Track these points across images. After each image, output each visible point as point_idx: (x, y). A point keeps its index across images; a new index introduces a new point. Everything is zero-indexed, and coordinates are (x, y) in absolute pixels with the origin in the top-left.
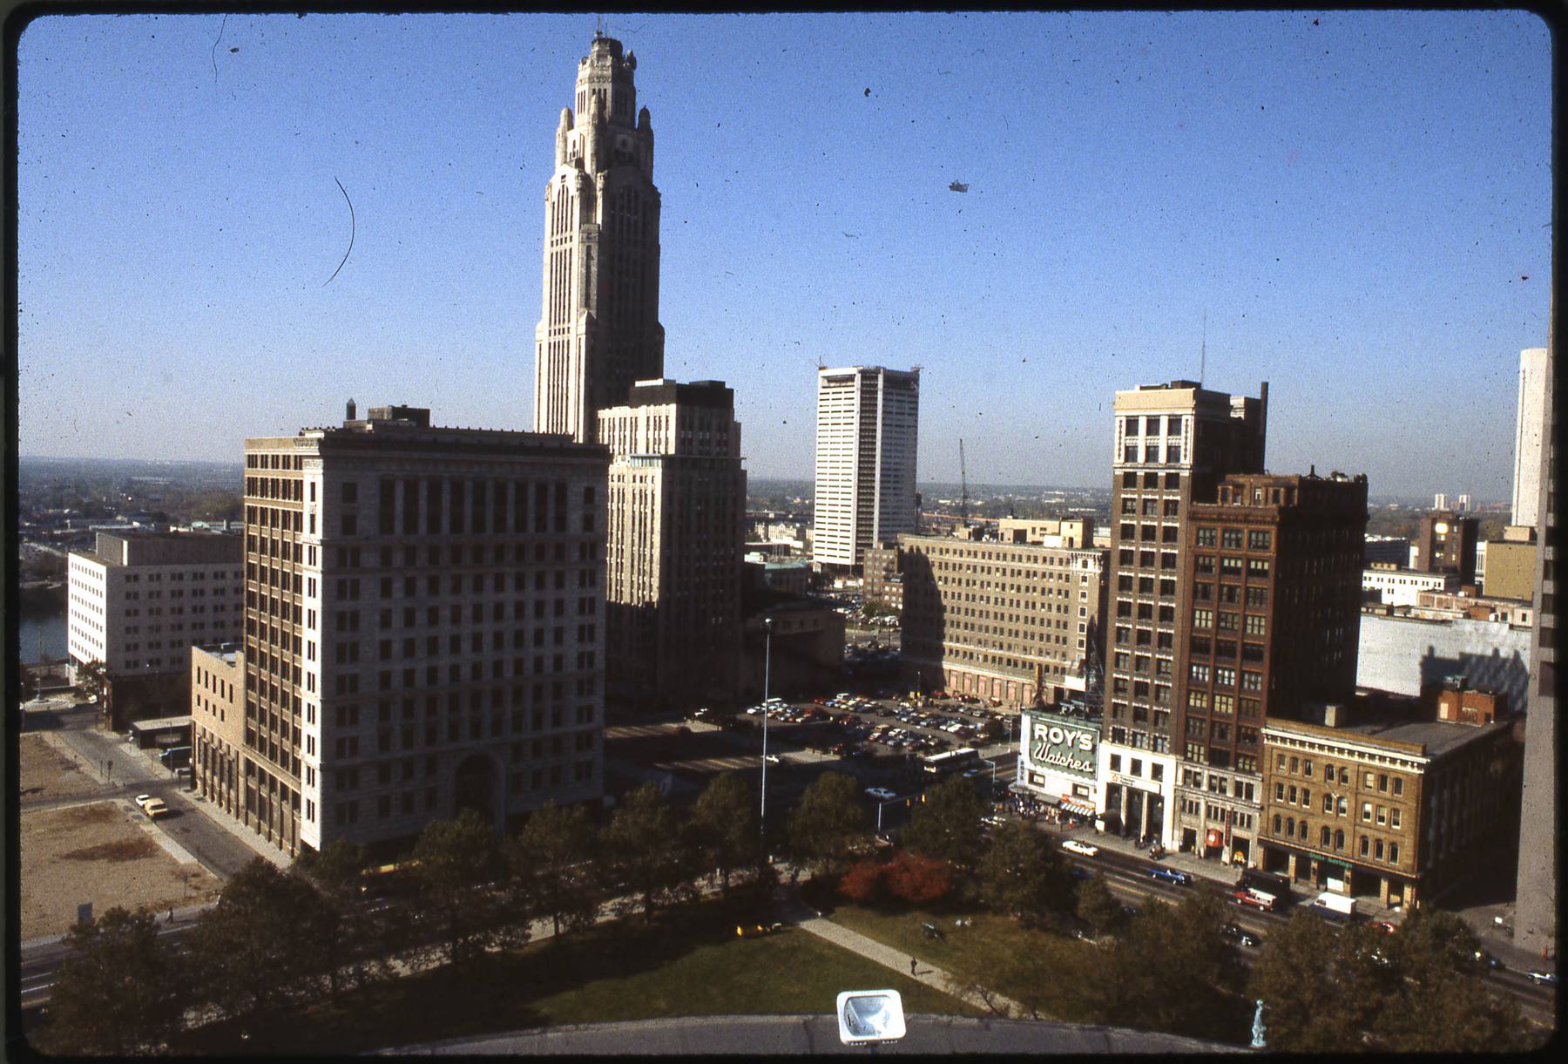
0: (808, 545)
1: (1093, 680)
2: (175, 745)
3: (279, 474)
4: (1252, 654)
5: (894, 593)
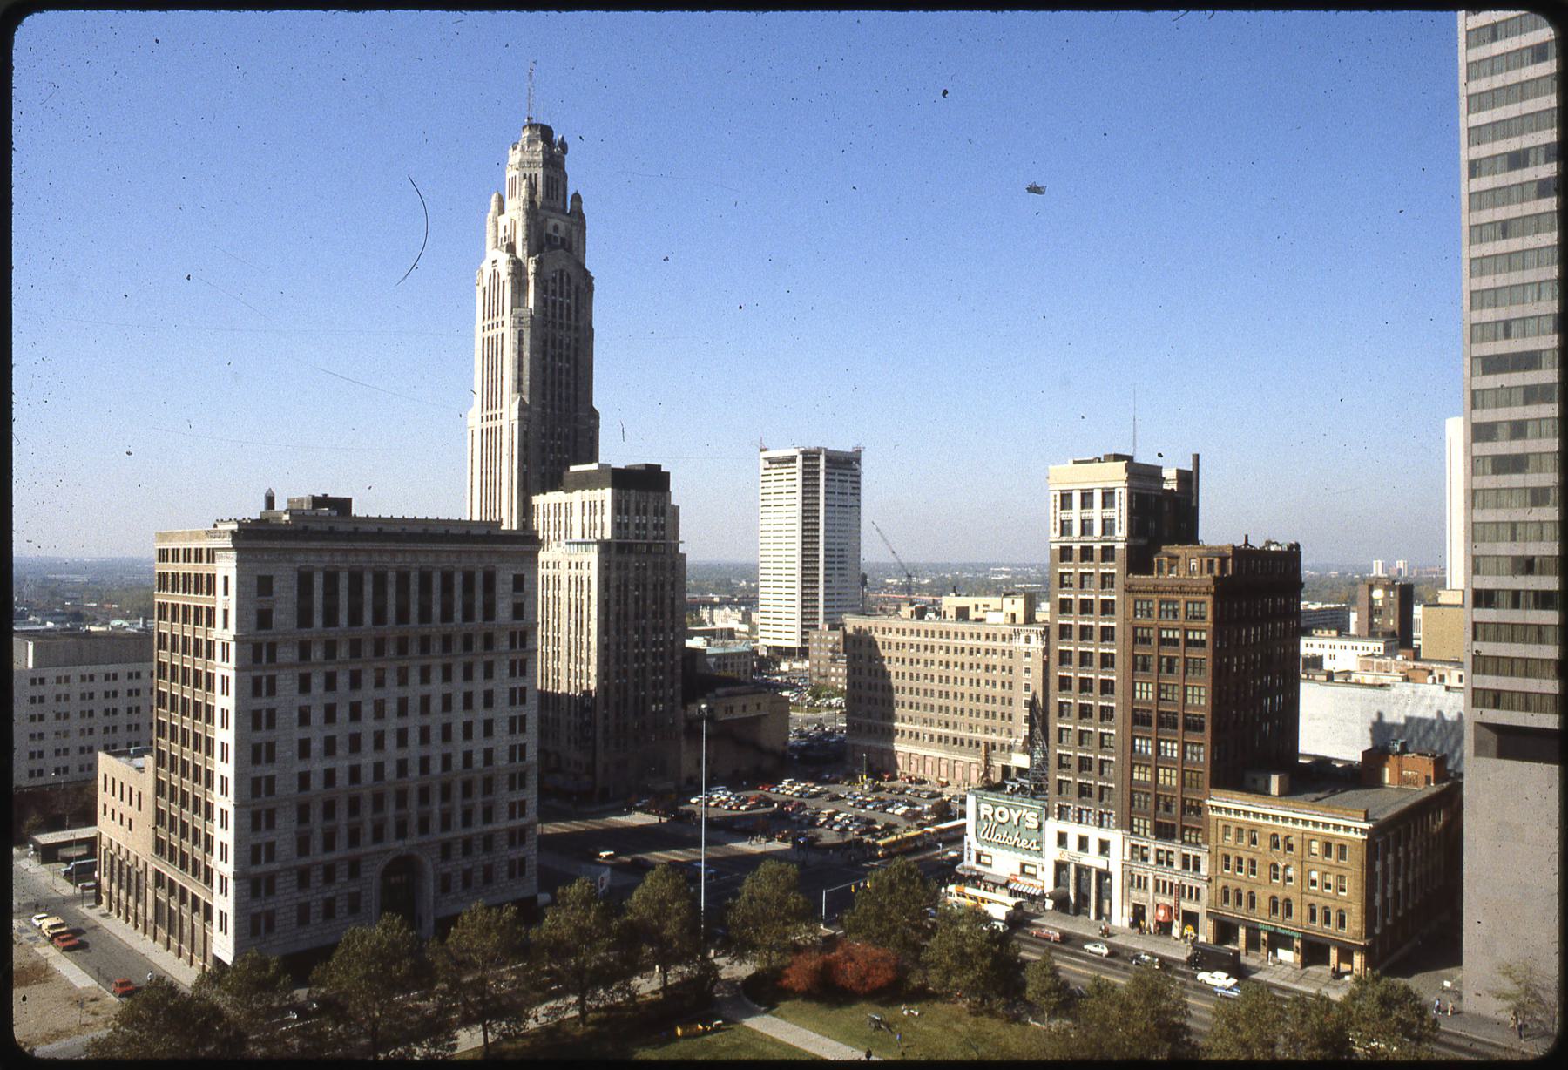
0: (753, 629)
1: (1038, 756)
2: (78, 858)
3: (191, 568)
4: (1193, 725)
5: (839, 676)
